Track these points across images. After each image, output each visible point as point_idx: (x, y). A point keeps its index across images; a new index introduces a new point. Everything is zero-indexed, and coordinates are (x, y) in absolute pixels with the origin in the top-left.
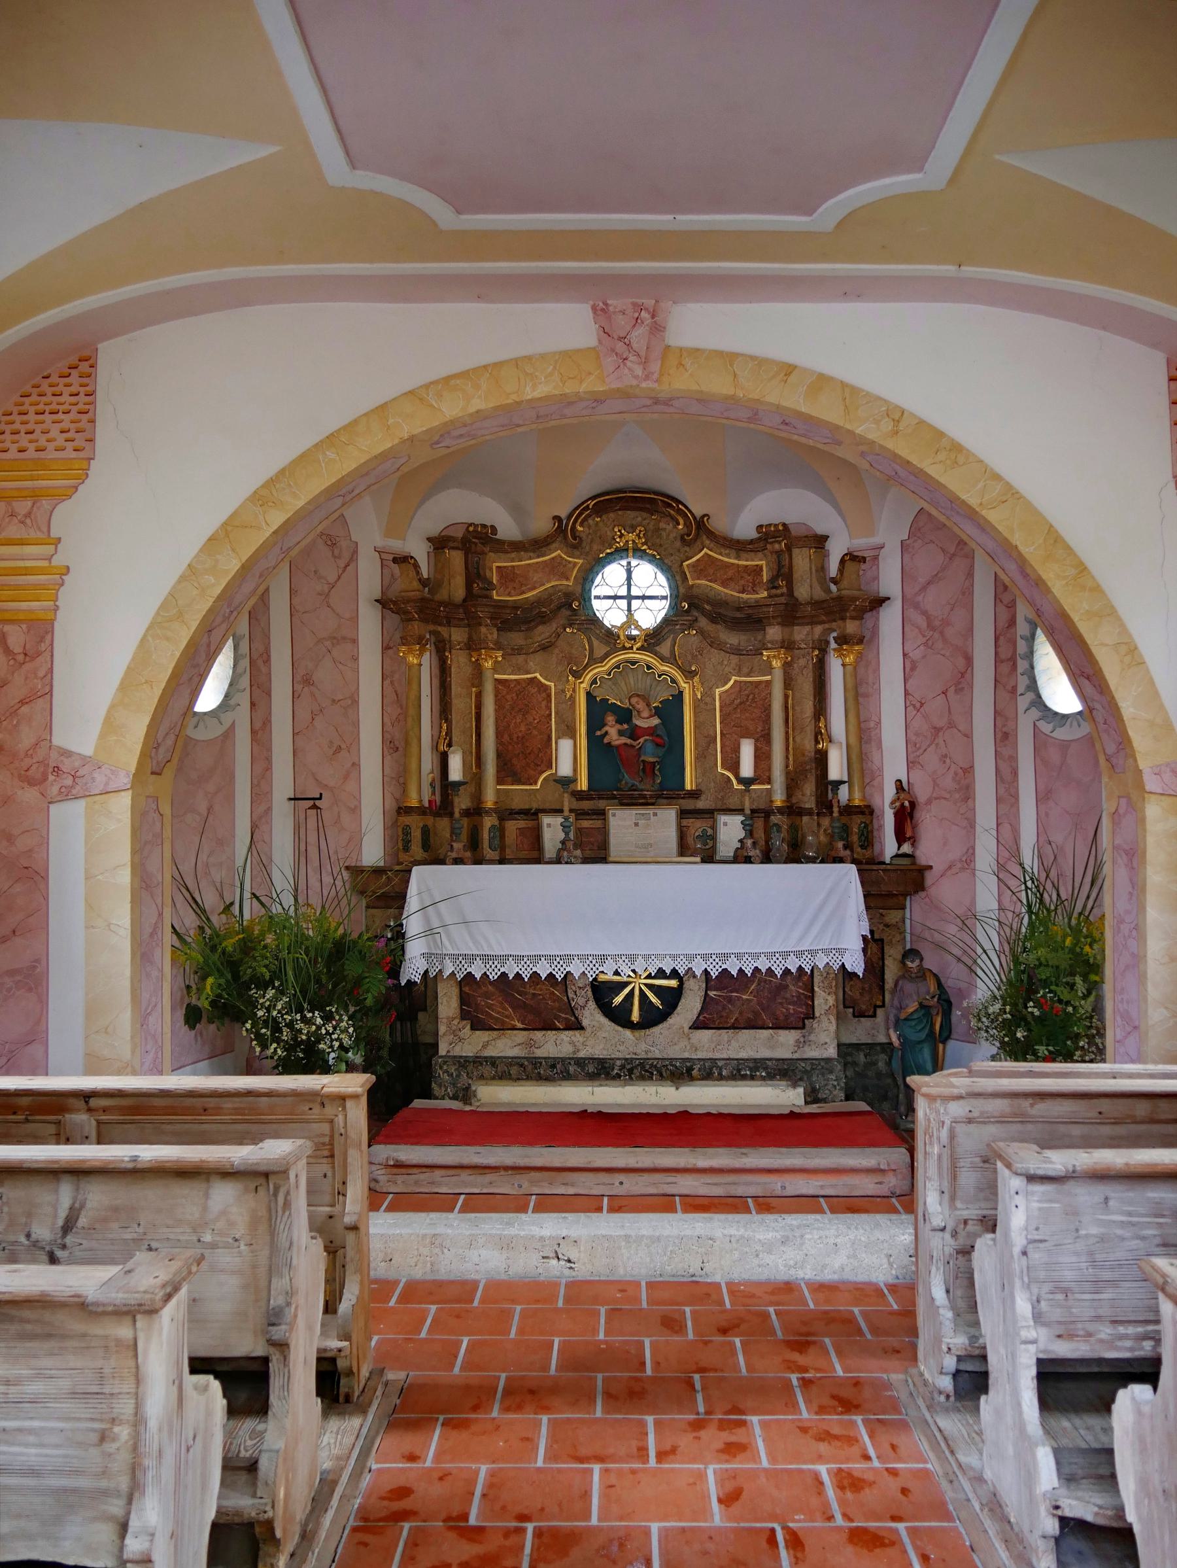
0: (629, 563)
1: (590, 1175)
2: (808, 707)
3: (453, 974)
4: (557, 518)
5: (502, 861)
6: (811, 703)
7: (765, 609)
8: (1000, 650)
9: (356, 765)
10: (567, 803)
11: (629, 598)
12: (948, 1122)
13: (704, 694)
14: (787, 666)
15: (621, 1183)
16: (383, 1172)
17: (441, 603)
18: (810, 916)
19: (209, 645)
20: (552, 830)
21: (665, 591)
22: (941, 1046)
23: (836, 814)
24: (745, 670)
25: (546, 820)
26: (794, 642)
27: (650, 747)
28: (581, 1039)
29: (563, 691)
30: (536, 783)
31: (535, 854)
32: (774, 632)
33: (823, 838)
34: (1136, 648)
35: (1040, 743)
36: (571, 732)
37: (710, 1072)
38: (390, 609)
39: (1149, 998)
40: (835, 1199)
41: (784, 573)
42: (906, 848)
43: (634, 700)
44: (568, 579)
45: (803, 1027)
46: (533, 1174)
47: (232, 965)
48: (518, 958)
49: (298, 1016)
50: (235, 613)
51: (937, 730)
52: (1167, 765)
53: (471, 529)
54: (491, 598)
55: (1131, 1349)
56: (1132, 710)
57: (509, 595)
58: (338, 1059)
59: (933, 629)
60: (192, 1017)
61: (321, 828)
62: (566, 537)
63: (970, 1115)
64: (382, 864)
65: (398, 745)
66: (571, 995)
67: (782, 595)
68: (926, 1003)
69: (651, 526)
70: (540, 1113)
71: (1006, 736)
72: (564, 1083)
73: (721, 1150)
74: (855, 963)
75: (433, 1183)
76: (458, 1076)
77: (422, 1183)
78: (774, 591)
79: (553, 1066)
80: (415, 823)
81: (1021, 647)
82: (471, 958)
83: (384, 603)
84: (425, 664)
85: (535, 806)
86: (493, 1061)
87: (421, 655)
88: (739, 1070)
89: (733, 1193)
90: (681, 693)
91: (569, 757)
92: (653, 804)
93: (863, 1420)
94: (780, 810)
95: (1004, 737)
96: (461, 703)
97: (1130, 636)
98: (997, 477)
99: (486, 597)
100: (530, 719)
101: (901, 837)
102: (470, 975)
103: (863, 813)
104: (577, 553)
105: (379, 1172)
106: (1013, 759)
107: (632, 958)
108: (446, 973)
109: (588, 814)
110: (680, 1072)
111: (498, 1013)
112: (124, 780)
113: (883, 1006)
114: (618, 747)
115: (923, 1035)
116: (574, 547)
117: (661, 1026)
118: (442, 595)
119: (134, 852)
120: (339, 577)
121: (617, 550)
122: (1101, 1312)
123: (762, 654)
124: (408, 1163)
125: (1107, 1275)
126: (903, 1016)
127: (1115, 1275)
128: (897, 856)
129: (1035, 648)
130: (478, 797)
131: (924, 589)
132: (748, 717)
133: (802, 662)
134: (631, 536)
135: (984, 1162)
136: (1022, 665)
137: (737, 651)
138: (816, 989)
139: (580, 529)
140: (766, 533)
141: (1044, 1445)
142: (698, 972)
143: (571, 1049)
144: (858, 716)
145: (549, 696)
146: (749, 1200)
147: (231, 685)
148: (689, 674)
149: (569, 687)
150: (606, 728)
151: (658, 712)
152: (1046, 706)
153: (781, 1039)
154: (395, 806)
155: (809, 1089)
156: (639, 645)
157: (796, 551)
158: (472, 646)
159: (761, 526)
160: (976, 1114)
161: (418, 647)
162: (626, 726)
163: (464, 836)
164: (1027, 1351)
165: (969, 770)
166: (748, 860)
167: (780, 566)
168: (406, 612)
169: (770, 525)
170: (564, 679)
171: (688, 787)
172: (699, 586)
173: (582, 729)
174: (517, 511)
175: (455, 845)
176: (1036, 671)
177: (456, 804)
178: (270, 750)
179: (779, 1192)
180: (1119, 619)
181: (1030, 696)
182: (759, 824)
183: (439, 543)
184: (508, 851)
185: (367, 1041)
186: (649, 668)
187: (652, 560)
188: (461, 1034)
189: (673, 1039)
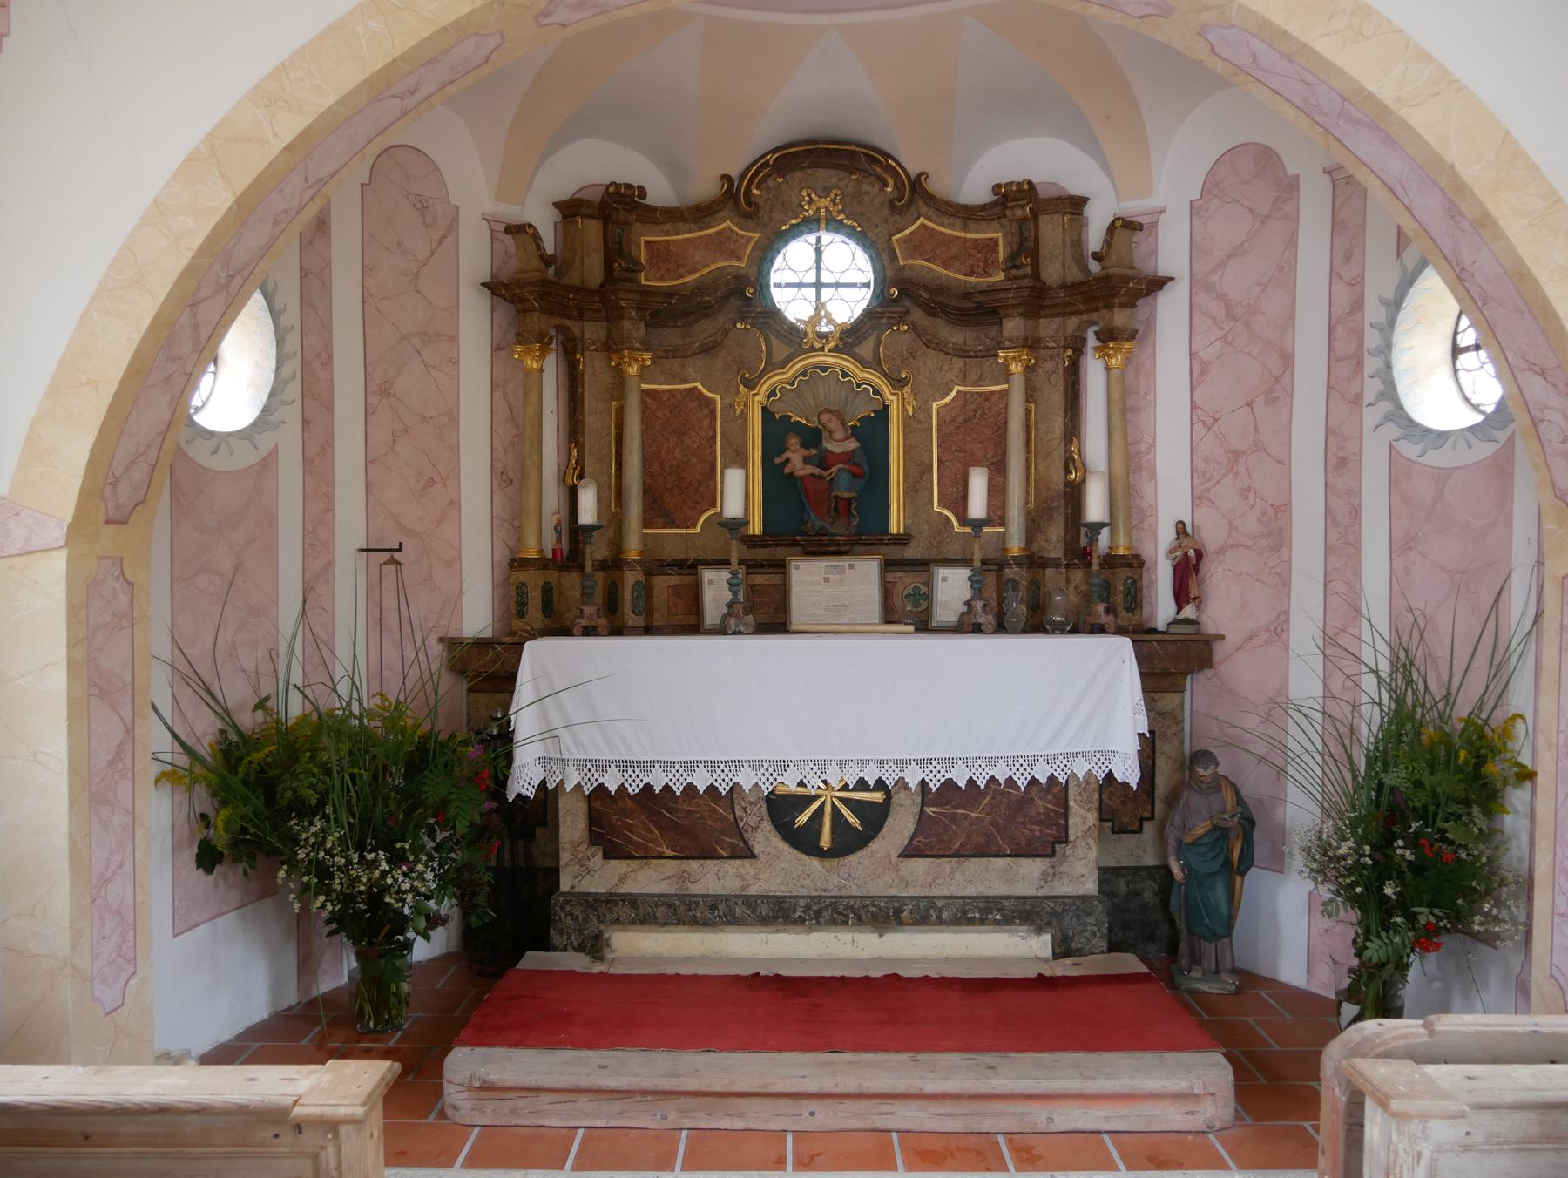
0: (819, 240)
1: (768, 1101)
2: (1057, 425)
3: (579, 786)
4: (726, 178)
5: (649, 631)
6: (1061, 420)
7: (1003, 295)
8: (1336, 344)
9: (455, 504)
10: (736, 552)
11: (818, 285)
12: (1427, 1153)
13: (917, 410)
14: (1029, 370)
15: (812, 1114)
16: (465, 1095)
17: (570, 288)
18: (1066, 706)
19: (196, 327)
20: (716, 588)
21: (869, 276)
22: (1238, 879)
23: (1095, 567)
24: (972, 377)
25: (708, 575)
26: (1039, 340)
27: (845, 479)
28: (752, 871)
29: (732, 406)
30: (694, 526)
31: (692, 620)
32: (1013, 326)
33: (1073, 598)
35: (1399, 473)
36: (741, 460)
37: (925, 914)
38: (501, 296)
40: (1126, 1136)
41: (1026, 248)
42: (1189, 612)
43: (825, 418)
44: (739, 258)
45: (1053, 854)
46: (683, 1100)
47: (265, 783)
48: (668, 765)
49: (355, 857)
50: (238, 281)
51: (1237, 455)
53: (611, 189)
54: (639, 282)
57: (662, 279)
58: (417, 909)
59: (1234, 319)
60: (207, 858)
61: (401, 588)
62: (737, 204)
63: (1468, 1140)
64: (488, 633)
65: (513, 476)
66: (738, 813)
67: (1025, 276)
68: (1222, 824)
69: (850, 190)
70: (696, 978)
71: (1343, 462)
72: (728, 928)
73: (956, 1058)
74: (1128, 772)
75: (537, 1112)
76: (586, 920)
77: (524, 1113)
78: (1014, 272)
79: (714, 907)
80: (533, 580)
81: (1372, 339)
82: (604, 765)
83: (495, 288)
84: (551, 369)
85: (693, 556)
86: (632, 900)
87: (542, 356)
88: (965, 913)
89: (975, 1127)
90: (886, 408)
91: (738, 493)
92: (847, 553)
94: (1018, 561)
95: (1341, 462)
96: (596, 421)
98: (1424, 57)
99: (631, 281)
100: (688, 442)
101: (1182, 595)
102: (601, 788)
103: (1130, 566)
104: (751, 224)
105: (459, 1096)
106: (1354, 494)
107: (823, 765)
108: (569, 787)
109: (762, 566)
110: (885, 915)
111: (640, 836)
112: (56, 533)
113: (1152, 818)
114: (803, 478)
115: (1216, 865)
116: (748, 216)
117: (860, 853)
118: (573, 278)
119: (72, 644)
120: (433, 253)
121: (806, 221)
123: (996, 356)
124: (500, 1084)
126: (1188, 839)
128: (1176, 622)
129: (1395, 339)
130: (617, 545)
131: (1223, 264)
132: (978, 437)
133: (1049, 365)
134: (824, 202)
136: (1372, 364)
137: (962, 353)
138: (1071, 803)
139: (756, 192)
140: (1004, 196)
142: (913, 783)
143: (738, 884)
144: (1125, 435)
145: (713, 412)
146: (1001, 1139)
147: (272, 394)
148: (898, 383)
149: (740, 400)
150: (788, 454)
151: (855, 433)
152: (1410, 420)
153: (1022, 871)
154: (507, 557)
155: (1060, 937)
156: (832, 344)
157: (1044, 220)
158: (611, 346)
159: (998, 186)
160: (1478, 1137)
161: (537, 346)
162: (813, 451)
163: (599, 597)
165: (1283, 509)
166: (977, 629)
167: (1023, 239)
168: (522, 300)
169: (1011, 183)
170: (733, 390)
171: (894, 529)
172: (912, 267)
173: (756, 454)
174: (673, 168)
175: (586, 610)
176: (1395, 373)
177: (587, 556)
178: (331, 483)
179: (1042, 1127)
181: (1385, 407)
182: (991, 579)
183: (570, 209)
184: (656, 616)
185: (457, 882)
186: (845, 375)
187: (851, 233)
188: (590, 864)
189: (875, 870)
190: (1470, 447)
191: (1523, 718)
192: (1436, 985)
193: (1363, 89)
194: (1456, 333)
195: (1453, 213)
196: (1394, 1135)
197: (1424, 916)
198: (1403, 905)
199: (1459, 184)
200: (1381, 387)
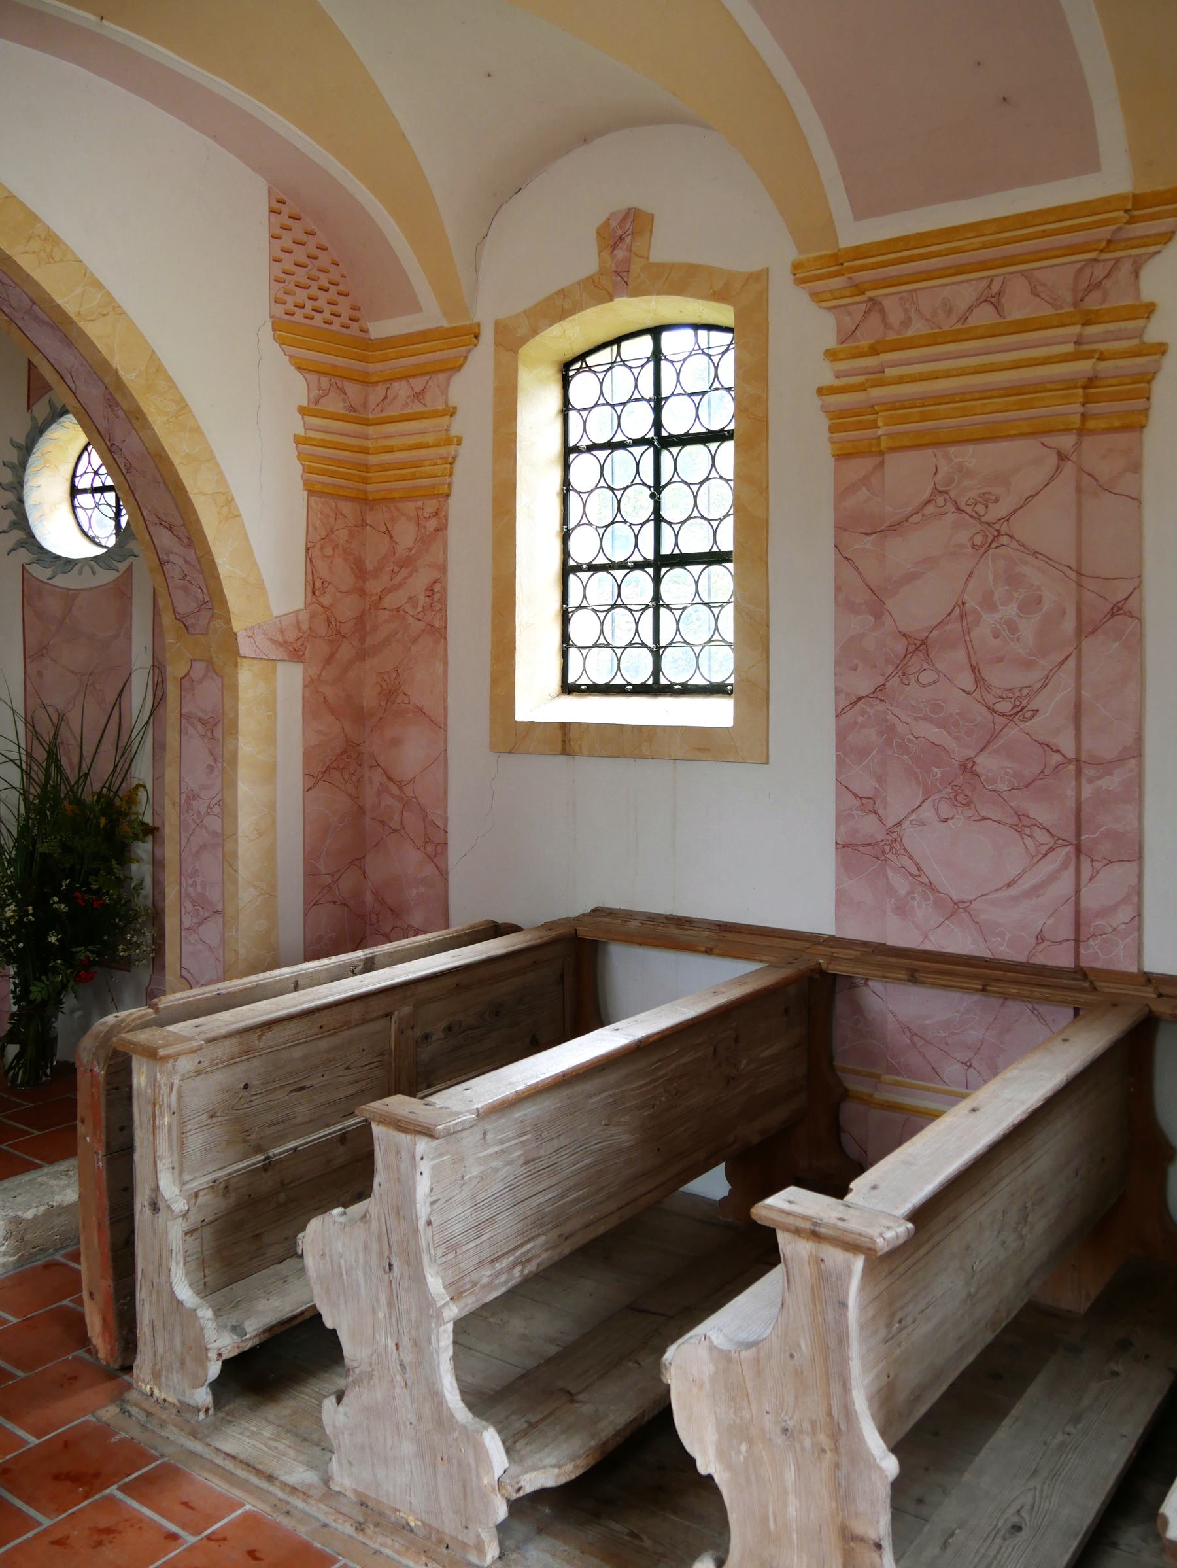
12: (176, 1082)
34: (233, 499)
39: (240, 879)
52: (260, 626)
55: (506, 1282)
56: (228, 567)
93: (119, 1489)
97: (228, 487)
98: (97, 284)
120: (1036, 553)
125: (486, 1214)
135: (212, 1117)
141: (485, 1428)
164: (445, 1331)
180: (218, 466)
181: (17, 535)
190: (94, 574)
191: (145, 787)
192: (78, 1014)
193: (53, 301)
194: (74, 476)
195: (112, 403)
196: (158, 1076)
197: (82, 953)
198: (63, 950)
199: (120, 384)
200: (14, 517)
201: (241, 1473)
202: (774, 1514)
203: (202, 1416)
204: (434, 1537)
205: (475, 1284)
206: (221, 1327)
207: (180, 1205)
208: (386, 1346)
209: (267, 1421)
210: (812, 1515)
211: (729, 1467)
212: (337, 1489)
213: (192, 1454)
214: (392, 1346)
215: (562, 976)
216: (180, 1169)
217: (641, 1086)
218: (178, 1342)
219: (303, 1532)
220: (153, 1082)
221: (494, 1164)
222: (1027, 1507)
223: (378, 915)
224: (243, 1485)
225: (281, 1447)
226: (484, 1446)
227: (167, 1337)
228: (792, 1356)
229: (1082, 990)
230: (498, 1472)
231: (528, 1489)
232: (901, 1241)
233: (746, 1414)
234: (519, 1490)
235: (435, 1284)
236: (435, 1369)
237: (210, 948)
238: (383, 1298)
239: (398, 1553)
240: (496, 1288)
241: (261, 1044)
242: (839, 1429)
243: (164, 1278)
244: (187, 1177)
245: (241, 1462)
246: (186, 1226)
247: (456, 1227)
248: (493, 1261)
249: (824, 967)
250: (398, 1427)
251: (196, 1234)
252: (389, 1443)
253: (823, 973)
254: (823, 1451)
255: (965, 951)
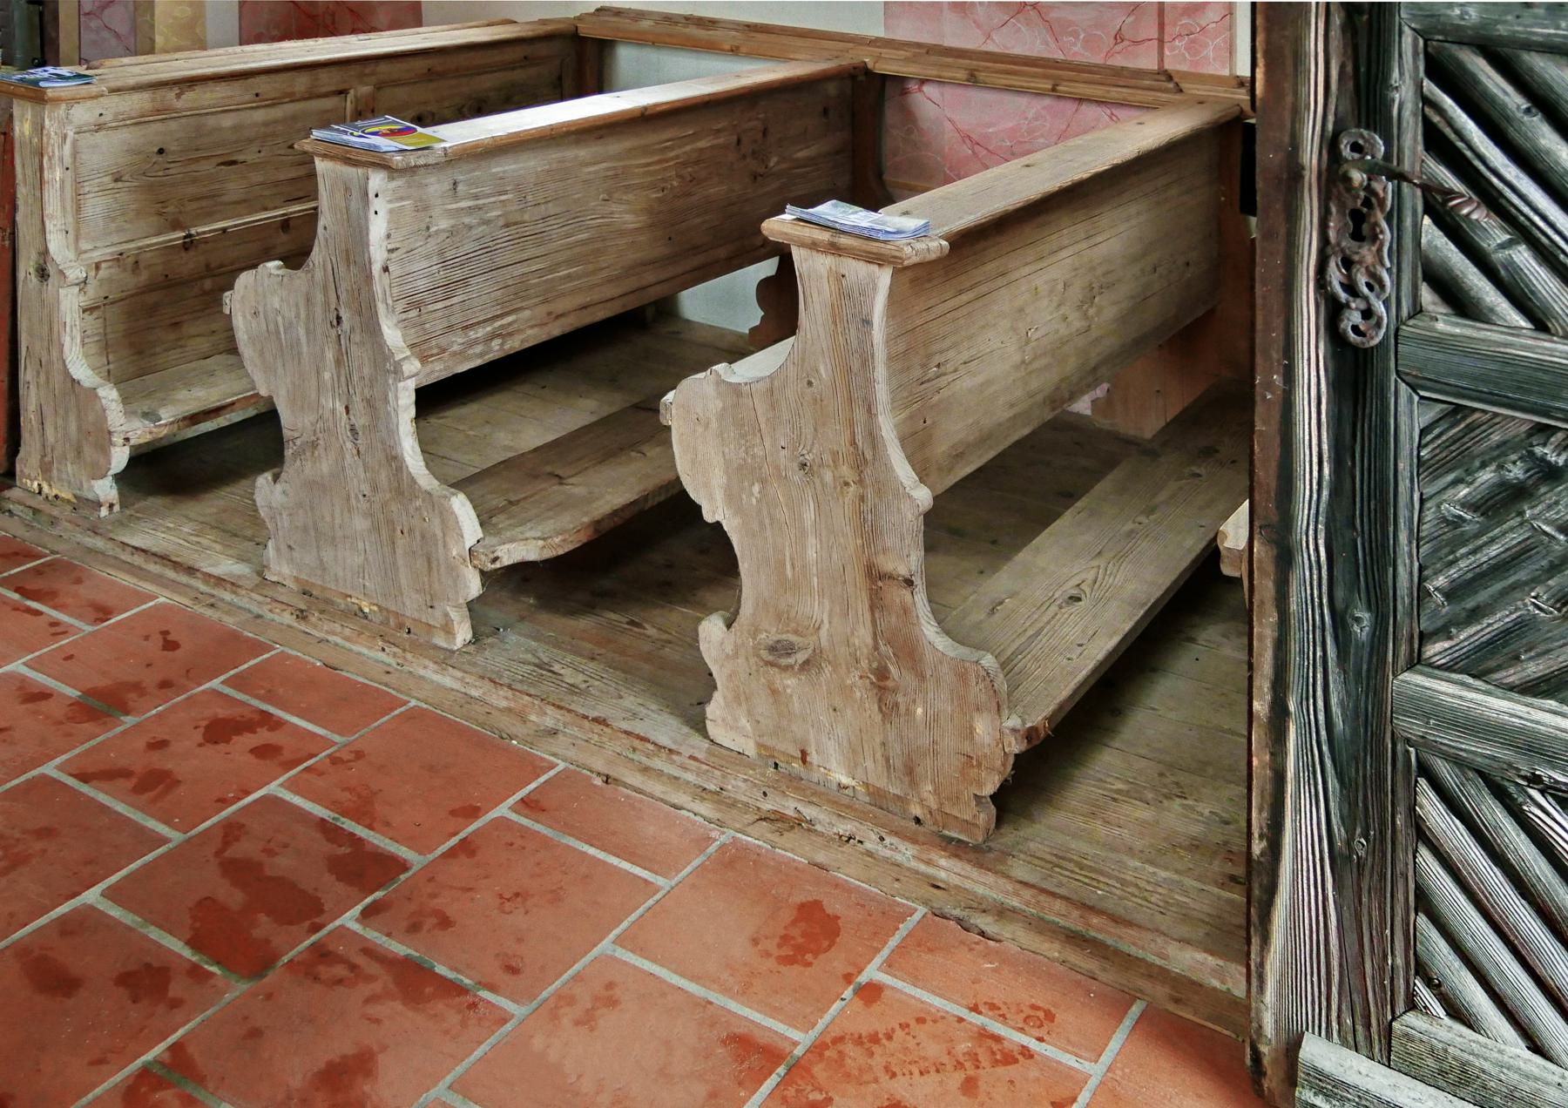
12: (71, 134)
55: (481, 355)
122: (453, 320)
125: (458, 274)
127: (465, 272)
135: (116, 180)
164: (405, 389)
196: (47, 122)
201: (154, 568)
202: (792, 559)
203: (104, 512)
204: (392, 622)
205: (444, 351)
206: (129, 414)
207: (75, 273)
208: (333, 411)
209: (186, 517)
210: (835, 556)
211: (739, 510)
212: (274, 579)
213: (91, 551)
214: (340, 408)
215: (560, 78)
216: (76, 234)
217: (648, 165)
218: (73, 427)
219: (230, 622)
220: (39, 128)
221: (467, 220)
222: (1089, 582)
223: (333, 15)
224: (158, 580)
225: (205, 542)
226: (453, 513)
227: (60, 422)
228: (810, 384)
229: (1166, 91)
230: (470, 541)
231: (507, 561)
232: (933, 256)
233: (758, 451)
234: (495, 560)
235: (392, 335)
236: (393, 432)
237: (117, 35)
238: (330, 355)
239: (347, 639)
240: (468, 359)
241: (179, 104)
242: (864, 459)
243: (55, 353)
244: (84, 246)
245: (154, 554)
246: (84, 301)
247: (419, 283)
248: (466, 327)
249: (870, 66)
250: (348, 499)
251: (96, 314)
252: (338, 521)
253: (867, 72)
254: (847, 484)
255: (1035, 54)
